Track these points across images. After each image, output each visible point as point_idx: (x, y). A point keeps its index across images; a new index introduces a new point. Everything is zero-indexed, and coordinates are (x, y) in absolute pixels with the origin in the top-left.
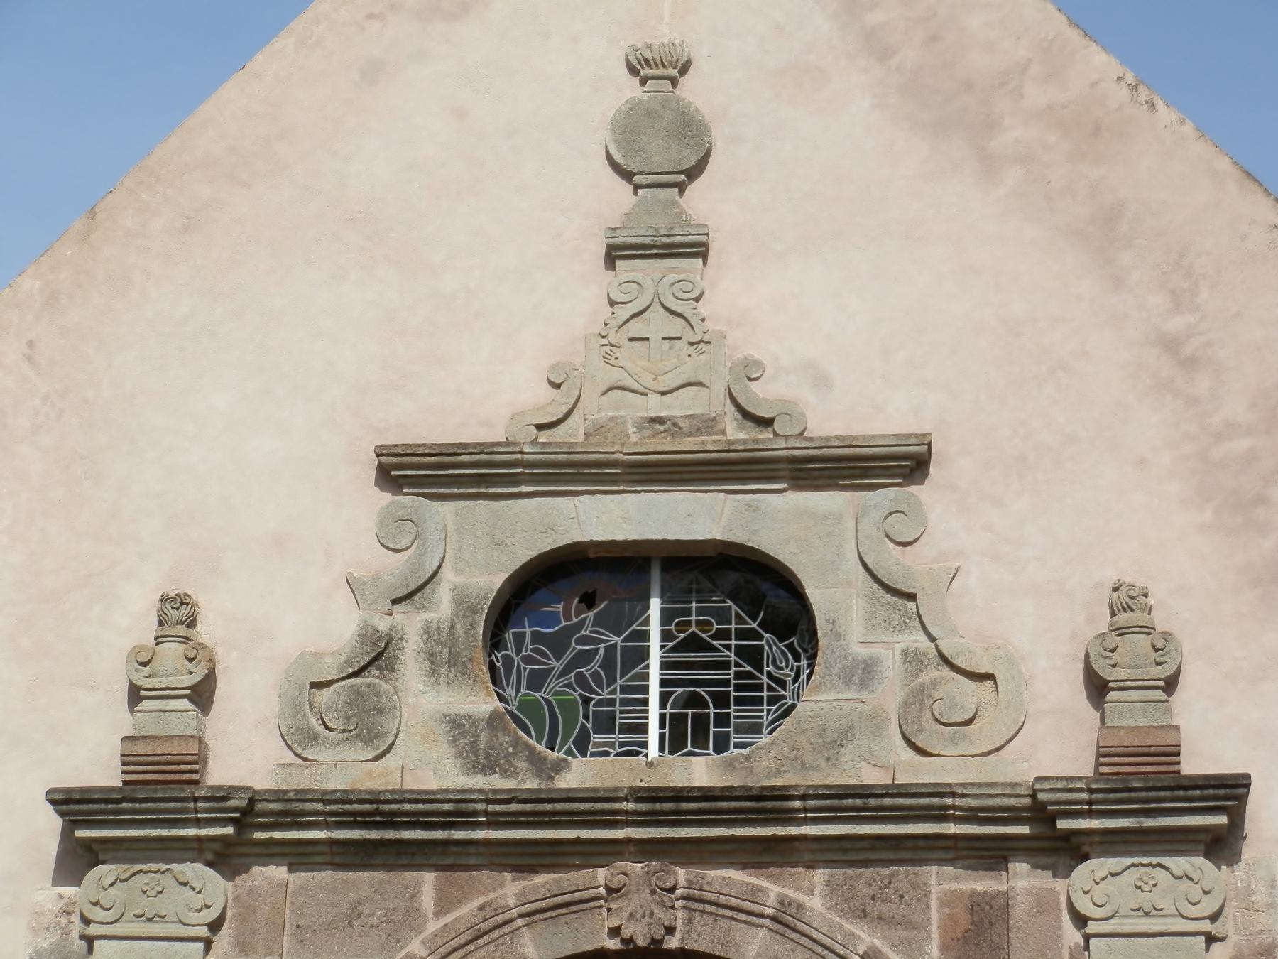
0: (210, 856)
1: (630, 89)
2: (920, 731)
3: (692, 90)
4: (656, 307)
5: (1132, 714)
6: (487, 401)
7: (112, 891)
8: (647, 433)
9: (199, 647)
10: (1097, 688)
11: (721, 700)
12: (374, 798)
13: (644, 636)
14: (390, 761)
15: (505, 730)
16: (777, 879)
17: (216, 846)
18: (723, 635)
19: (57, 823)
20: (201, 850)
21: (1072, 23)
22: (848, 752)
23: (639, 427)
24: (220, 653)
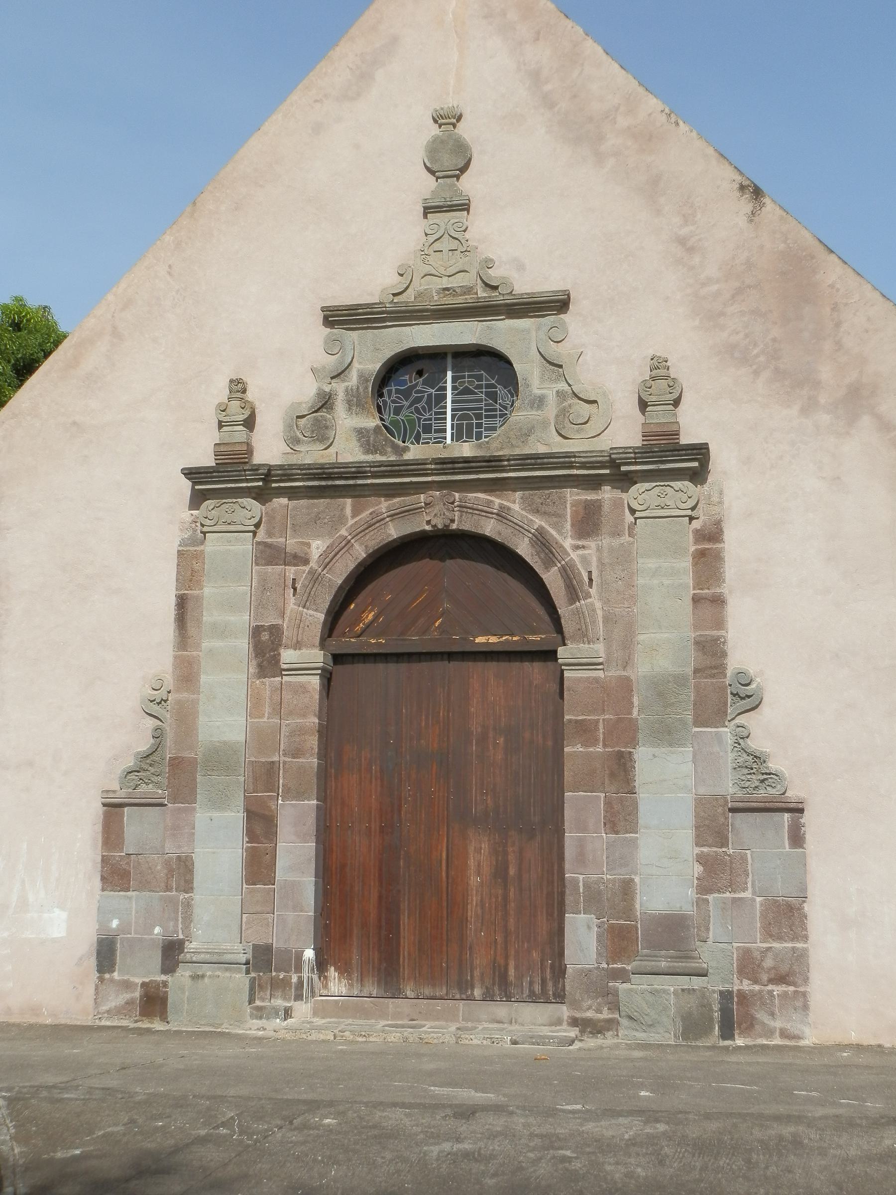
0: (254, 495)
1: (435, 130)
2: (564, 428)
3: (464, 130)
4: (446, 236)
5: (659, 416)
6: (371, 284)
7: (213, 512)
8: (442, 295)
9: (246, 402)
10: (643, 405)
11: (478, 417)
12: (322, 467)
13: (445, 389)
14: (332, 450)
15: (382, 434)
16: (498, 497)
17: (256, 490)
18: (479, 387)
19: (189, 483)
20: (250, 493)
21: (640, 84)
22: (532, 438)
23: (438, 293)
24: (257, 404)
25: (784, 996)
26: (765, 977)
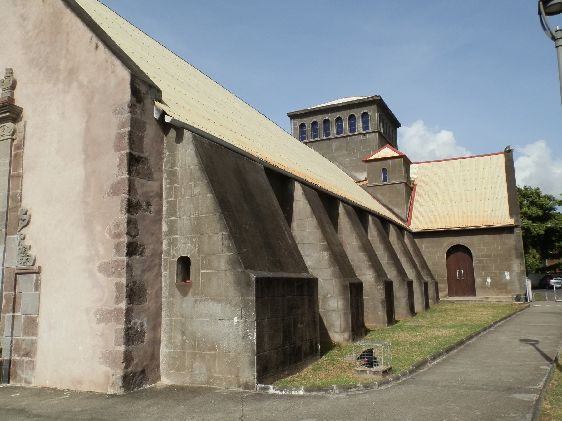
25: (27, 362)
26: (22, 353)
